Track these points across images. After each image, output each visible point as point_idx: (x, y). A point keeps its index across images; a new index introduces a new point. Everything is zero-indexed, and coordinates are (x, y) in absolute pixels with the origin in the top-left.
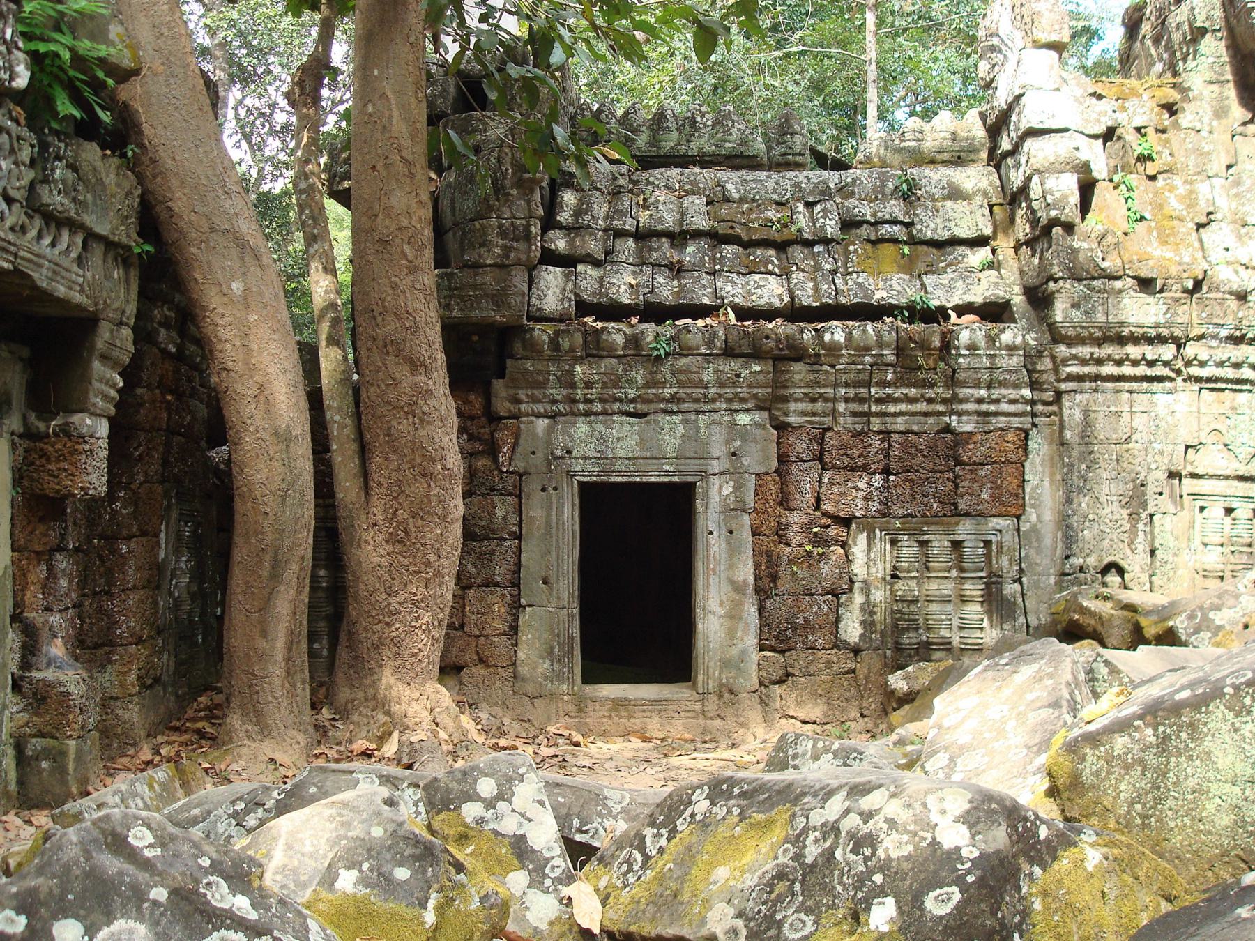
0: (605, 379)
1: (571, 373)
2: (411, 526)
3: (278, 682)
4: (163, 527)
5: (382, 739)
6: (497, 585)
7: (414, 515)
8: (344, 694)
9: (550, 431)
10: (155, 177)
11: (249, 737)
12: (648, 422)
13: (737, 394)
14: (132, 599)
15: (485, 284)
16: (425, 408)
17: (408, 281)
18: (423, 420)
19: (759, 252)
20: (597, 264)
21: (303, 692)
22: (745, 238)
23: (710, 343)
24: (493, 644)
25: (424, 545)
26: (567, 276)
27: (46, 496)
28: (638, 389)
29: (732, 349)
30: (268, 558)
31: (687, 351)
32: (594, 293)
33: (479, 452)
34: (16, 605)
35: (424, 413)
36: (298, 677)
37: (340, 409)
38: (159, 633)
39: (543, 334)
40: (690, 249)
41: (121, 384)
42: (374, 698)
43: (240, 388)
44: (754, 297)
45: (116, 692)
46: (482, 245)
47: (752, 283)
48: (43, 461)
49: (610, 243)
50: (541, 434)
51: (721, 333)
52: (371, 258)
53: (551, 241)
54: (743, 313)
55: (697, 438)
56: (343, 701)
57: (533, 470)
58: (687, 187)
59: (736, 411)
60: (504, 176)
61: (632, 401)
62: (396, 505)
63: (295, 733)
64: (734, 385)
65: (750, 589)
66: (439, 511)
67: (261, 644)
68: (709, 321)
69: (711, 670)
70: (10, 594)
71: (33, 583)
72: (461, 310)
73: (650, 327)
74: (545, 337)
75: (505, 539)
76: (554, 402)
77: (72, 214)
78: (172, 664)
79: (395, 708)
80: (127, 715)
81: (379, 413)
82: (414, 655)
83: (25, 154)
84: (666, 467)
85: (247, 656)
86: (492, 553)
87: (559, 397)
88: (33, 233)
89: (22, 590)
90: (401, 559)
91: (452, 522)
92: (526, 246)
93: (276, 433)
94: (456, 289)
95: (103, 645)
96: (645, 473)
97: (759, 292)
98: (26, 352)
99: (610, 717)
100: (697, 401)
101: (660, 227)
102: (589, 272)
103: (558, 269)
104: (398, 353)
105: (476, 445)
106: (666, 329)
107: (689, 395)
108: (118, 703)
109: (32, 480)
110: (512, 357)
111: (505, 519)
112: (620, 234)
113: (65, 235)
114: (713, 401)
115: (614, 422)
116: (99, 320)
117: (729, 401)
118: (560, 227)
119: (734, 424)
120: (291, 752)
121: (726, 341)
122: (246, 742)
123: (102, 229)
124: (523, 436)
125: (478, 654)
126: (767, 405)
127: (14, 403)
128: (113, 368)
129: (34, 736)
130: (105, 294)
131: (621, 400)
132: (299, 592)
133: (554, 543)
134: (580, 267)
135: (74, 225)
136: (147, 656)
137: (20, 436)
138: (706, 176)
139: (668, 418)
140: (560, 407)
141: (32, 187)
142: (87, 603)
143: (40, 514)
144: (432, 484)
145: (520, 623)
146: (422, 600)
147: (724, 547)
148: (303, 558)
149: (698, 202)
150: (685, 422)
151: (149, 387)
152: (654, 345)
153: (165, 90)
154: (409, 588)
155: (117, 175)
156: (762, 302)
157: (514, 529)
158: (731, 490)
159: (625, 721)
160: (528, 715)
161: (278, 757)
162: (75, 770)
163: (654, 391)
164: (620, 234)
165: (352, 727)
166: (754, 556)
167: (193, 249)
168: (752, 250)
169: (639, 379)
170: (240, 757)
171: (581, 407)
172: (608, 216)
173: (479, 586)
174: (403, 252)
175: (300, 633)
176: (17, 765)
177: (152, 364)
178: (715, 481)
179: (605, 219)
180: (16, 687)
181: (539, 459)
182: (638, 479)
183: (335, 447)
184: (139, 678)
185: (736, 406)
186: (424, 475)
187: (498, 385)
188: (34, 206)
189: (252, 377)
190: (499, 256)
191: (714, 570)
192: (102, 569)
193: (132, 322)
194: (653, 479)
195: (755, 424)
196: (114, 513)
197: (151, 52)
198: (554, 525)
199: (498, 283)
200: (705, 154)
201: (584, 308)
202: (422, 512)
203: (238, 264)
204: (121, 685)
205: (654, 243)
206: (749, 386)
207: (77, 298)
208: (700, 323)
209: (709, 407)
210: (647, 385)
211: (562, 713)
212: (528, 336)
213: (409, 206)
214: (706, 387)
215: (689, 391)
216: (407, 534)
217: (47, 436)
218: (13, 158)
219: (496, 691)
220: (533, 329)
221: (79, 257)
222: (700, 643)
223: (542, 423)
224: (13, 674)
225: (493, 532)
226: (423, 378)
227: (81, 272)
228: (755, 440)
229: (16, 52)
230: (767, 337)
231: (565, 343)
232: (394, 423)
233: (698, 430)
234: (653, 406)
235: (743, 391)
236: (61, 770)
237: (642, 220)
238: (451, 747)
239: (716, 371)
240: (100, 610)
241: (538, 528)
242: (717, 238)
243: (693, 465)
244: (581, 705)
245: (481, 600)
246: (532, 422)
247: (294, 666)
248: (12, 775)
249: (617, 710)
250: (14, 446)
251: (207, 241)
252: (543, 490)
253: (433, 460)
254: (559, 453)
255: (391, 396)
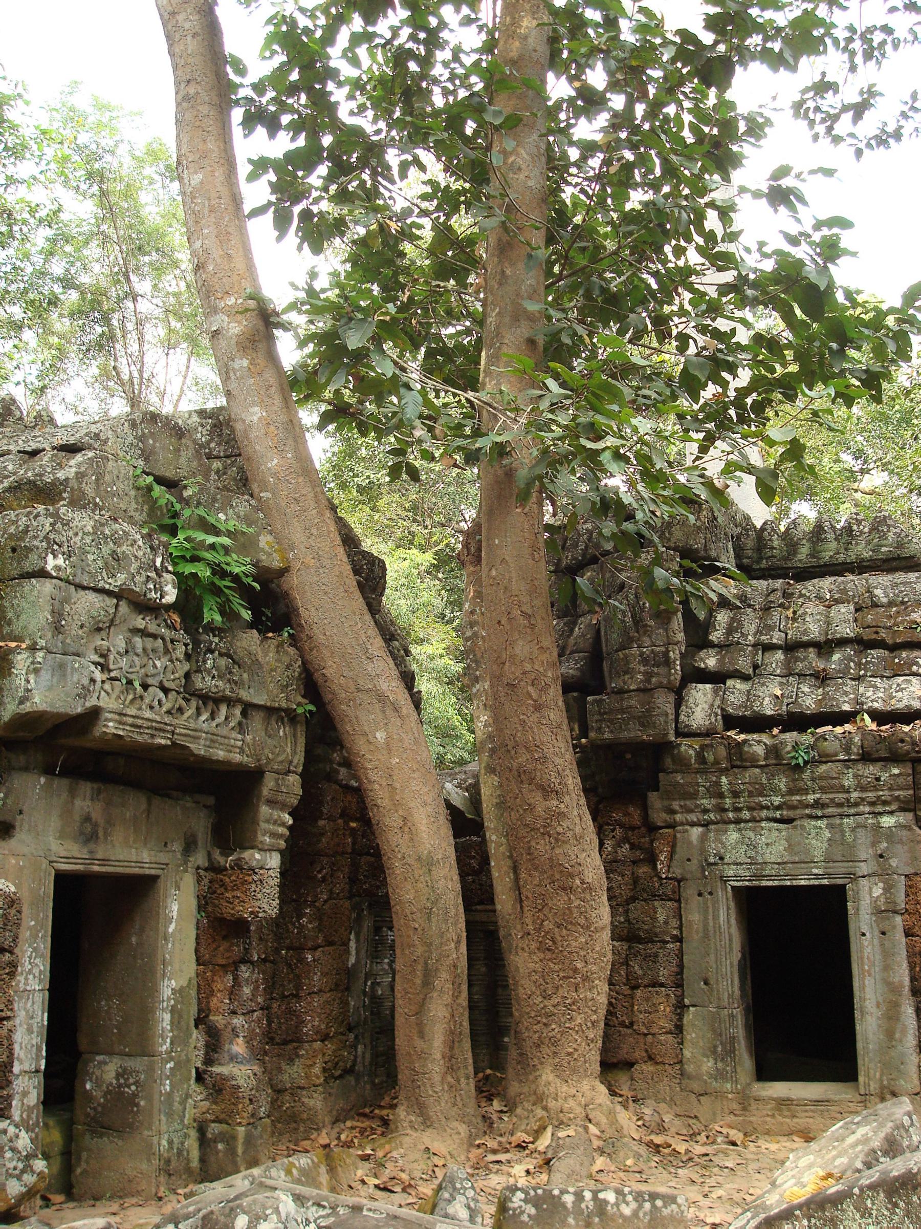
0: (751, 789)
1: (718, 784)
2: (557, 936)
3: (437, 1078)
4: (352, 937)
5: (538, 1133)
6: (662, 985)
7: (559, 926)
8: (514, 1088)
9: (703, 838)
10: (311, 650)
11: (412, 1127)
12: (795, 827)
13: (879, 797)
14: (316, 1001)
15: (631, 707)
16: (560, 829)
17: (535, 717)
18: (559, 839)
19: (904, 654)
20: (745, 678)
21: (468, 1086)
22: (890, 641)
23: (847, 749)
24: (659, 1042)
25: (570, 953)
26: (716, 692)
27: (225, 919)
28: (782, 796)
29: (869, 754)
30: (420, 967)
31: (825, 758)
32: (740, 706)
33: (640, 860)
34: (200, 1011)
35: (559, 834)
36: (462, 1073)
37: (496, 830)
38: (350, 1029)
39: (688, 748)
40: (836, 657)
41: (291, 822)
42: (535, 1093)
43: (387, 821)
44: (893, 702)
45: (303, 1082)
46: (626, 673)
47: (894, 686)
48: (222, 889)
49: (759, 657)
50: (695, 842)
51: (857, 739)
52: (502, 700)
53: (702, 660)
54: (880, 717)
55: (843, 842)
56: (512, 1094)
57: (688, 876)
58: (837, 596)
59: (880, 814)
60: (642, 609)
61: (778, 808)
62: (542, 917)
63: (455, 1124)
64: (876, 789)
65: (906, 990)
66: (582, 921)
67: (419, 1044)
68: (848, 727)
69: (872, 1072)
70: (195, 1002)
71: (219, 991)
72: (612, 732)
73: (790, 737)
74: (691, 752)
75: (667, 942)
76: (706, 811)
77: (228, 693)
78: (368, 1056)
79: (552, 1104)
80: (311, 1103)
81: (520, 835)
82: (569, 1054)
83: (180, 652)
84: (815, 871)
85: (409, 1053)
86: (656, 956)
87: (709, 807)
88: (190, 712)
89: (207, 998)
90: (552, 965)
91: (596, 930)
92: (666, 669)
93: (419, 859)
94: (605, 713)
95: (292, 1041)
96: (794, 877)
97: (900, 694)
98: (211, 801)
99: (773, 1116)
100: (840, 805)
101: (805, 638)
102: (738, 686)
103: (708, 686)
104: (531, 780)
105: (638, 853)
106: (807, 738)
107: (832, 800)
108: (304, 1092)
109: (215, 906)
110: (664, 771)
111: (666, 923)
112: (769, 648)
113: (223, 709)
114: (856, 805)
115: (762, 828)
116: (264, 772)
117: (872, 804)
118: (712, 645)
119: (878, 827)
120: (449, 1142)
121: (862, 747)
122: (409, 1131)
123: (260, 700)
124: (679, 844)
125: (647, 1051)
126: (912, 806)
127: (200, 843)
128: (282, 810)
129: (214, 1121)
130: (266, 751)
131: (767, 808)
132: (455, 997)
133: (712, 946)
134: (730, 683)
135: (231, 702)
136: (334, 1051)
137: (206, 870)
138: (853, 582)
139: (813, 823)
140: (712, 815)
141: (187, 675)
142: (275, 1005)
143: (224, 933)
144: (572, 897)
145: (685, 1022)
146: (573, 1003)
147: (877, 949)
148: (455, 966)
149: (845, 611)
150: (830, 827)
151: (331, 819)
152: (793, 754)
153: (315, 579)
154: (561, 992)
155: (278, 652)
156: (900, 705)
157: (675, 932)
158: (881, 891)
159: (788, 1120)
160: (695, 1112)
161: (436, 1146)
162: (244, 1153)
163: (798, 798)
164: (769, 648)
165: (515, 1119)
166: (908, 957)
167: (343, 707)
168: (897, 653)
169: (782, 786)
170: (401, 1144)
171: (731, 815)
172: (758, 632)
173: (646, 986)
174: (528, 693)
175: (460, 1033)
176: (201, 1145)
177: (333, 799)
178: (863, 882)
179: (755, 635)
180: (200, 1078)
181: (694, 865)
182: (788, 883)
183: (493, 864)
184: (324, 1070)
185: (880, 809)
186: (564, 889)
187: (653, 797)
188: (189, 692)
189: (397, 811)
190: (642, 681)
191: (869, 971)
192: (291, 976)
193: (300, 769)
194: (803, 883)
195: (899, 826)
196: (302, 927)
197: (304, 550)
198: (711, 928)
199: (643, 706)
200: (863, 560)
201: (730, 722)
202: (566, 922)
203: (381, 716)
204: (307, 1077)
205: (800, 654)
206: (890, 789)
207: (237, 758)
208: (839, 730)
209: (853, 811)
210: (791, 792)
211: (726, 1111)
212: (676, 752)
213: (531, 653)
214: (848, 792)
215: (831, 796)
216: (554, 943)
217: (226, 869)
218: (168, 657)
219: (664, 1087)
220: (680, 745)
221: (240, 724)
222: (860, 1045)
223: (696, 832)
224: (197, 1069)
225: (656, 935)
226: (555, 803)
227: (240, 737)
228: (901, 842)
229: (164, 574)
230: (902, 741)
231: (710, 757)
232: (533, 843)
233: (843, 833)
234: (798, 812)
235: (884, 794)
236: (232, 1151)
237: (790, 633)
238: (601, 1143)
239: (856, 776)
240: (290, 1012)
241: (697, 932)
242: (863, 644)
243: (841, 868)
244: (745, 1102)
245: (647, 999)
246: (687, 831)
247: (457, 1063)
248: (195, 1154)
249: (780, 1110)
250: (199, 880)
251: (354, 700)
252: (700, 895)
253: (571, 875)
254: (712, 860)
255: (529, 819)
